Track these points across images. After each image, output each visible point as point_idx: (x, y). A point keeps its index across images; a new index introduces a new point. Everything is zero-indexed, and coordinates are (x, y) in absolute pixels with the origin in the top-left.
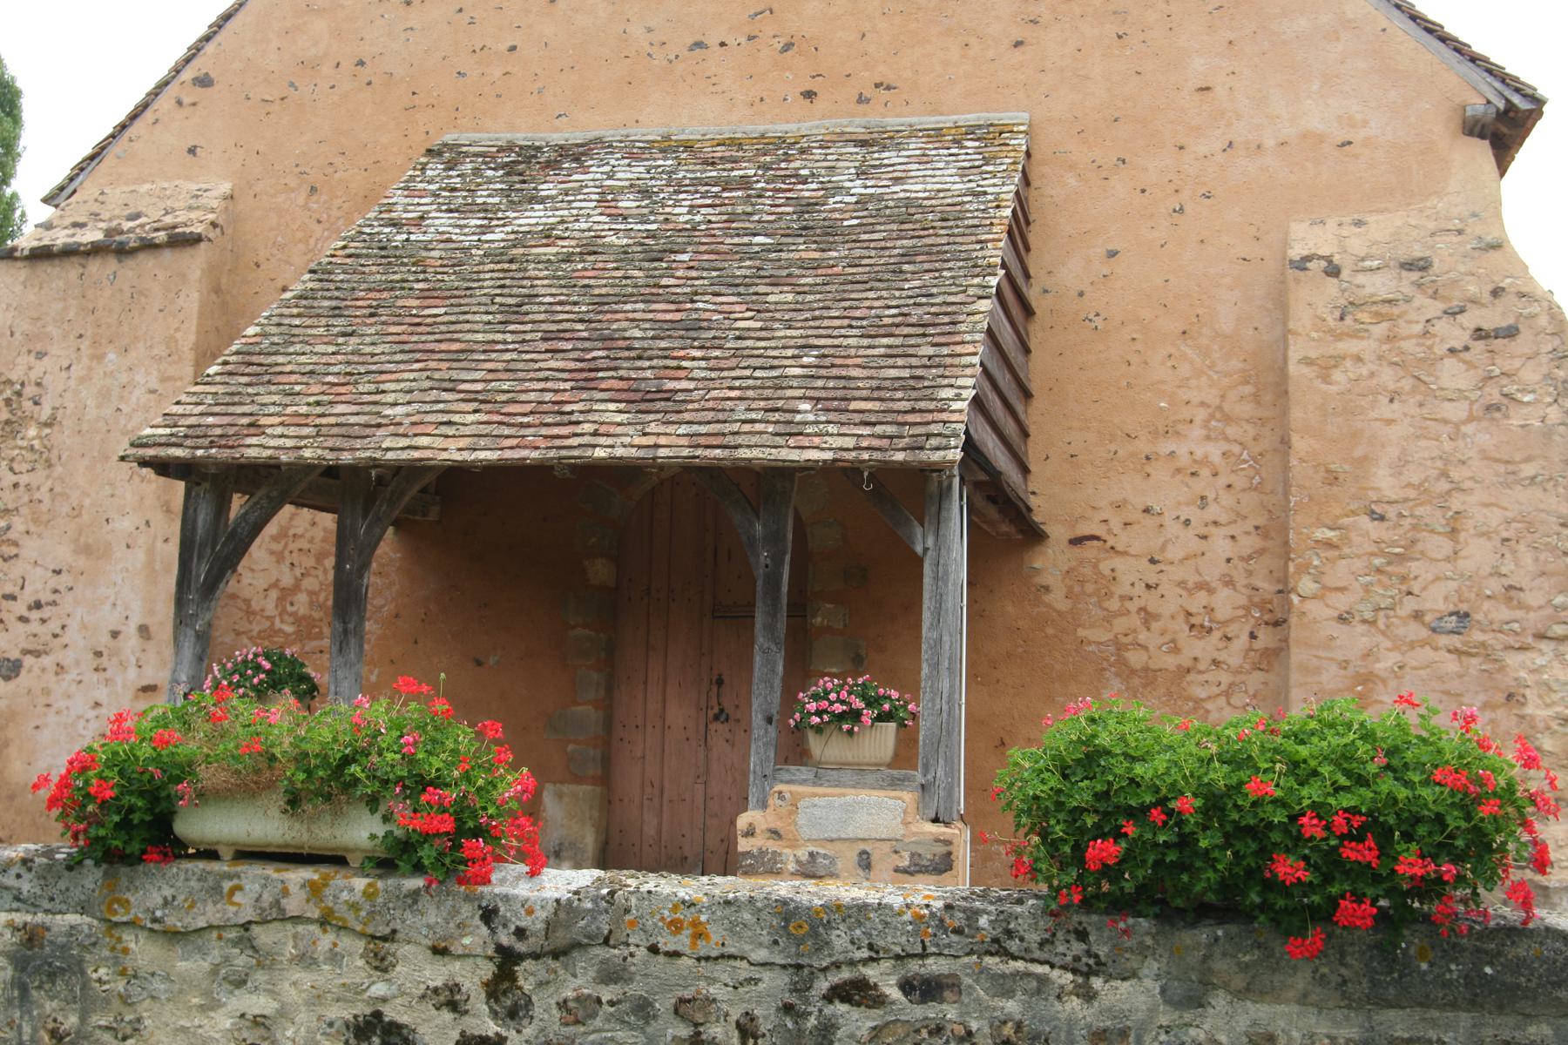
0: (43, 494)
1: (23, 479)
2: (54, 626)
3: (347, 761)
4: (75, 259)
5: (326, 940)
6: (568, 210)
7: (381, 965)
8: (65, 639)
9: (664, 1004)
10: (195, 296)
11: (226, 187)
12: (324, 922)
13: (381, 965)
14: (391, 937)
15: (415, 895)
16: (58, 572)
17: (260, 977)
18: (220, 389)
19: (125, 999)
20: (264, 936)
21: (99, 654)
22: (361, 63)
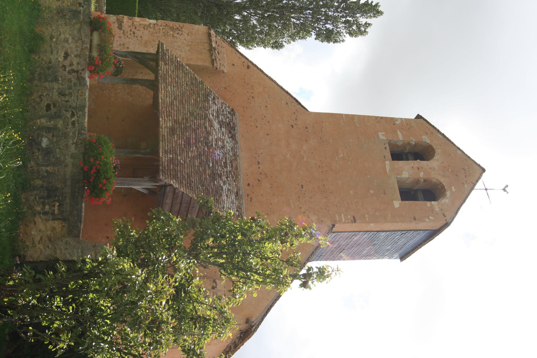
0: (158, 35)
1: (161, 31)
2: (129, 36)
3: (105, 52)
4: (208, 42)
5: (79, 49)
6: (217, 133)
7: (76, 56)
8: (127, 38)
9: (71, 91)
10: (201, 64)
11: (225, 71)
12: (82, 49)
13: (76, 56)
14: (80, 57)
15: (86, 60)
16: (141, 37)
17: (74, 41)
18: (174, 60)
19: (70, 24)
20: (80, 41)
21: (123, 45)
22: (253, 97)
